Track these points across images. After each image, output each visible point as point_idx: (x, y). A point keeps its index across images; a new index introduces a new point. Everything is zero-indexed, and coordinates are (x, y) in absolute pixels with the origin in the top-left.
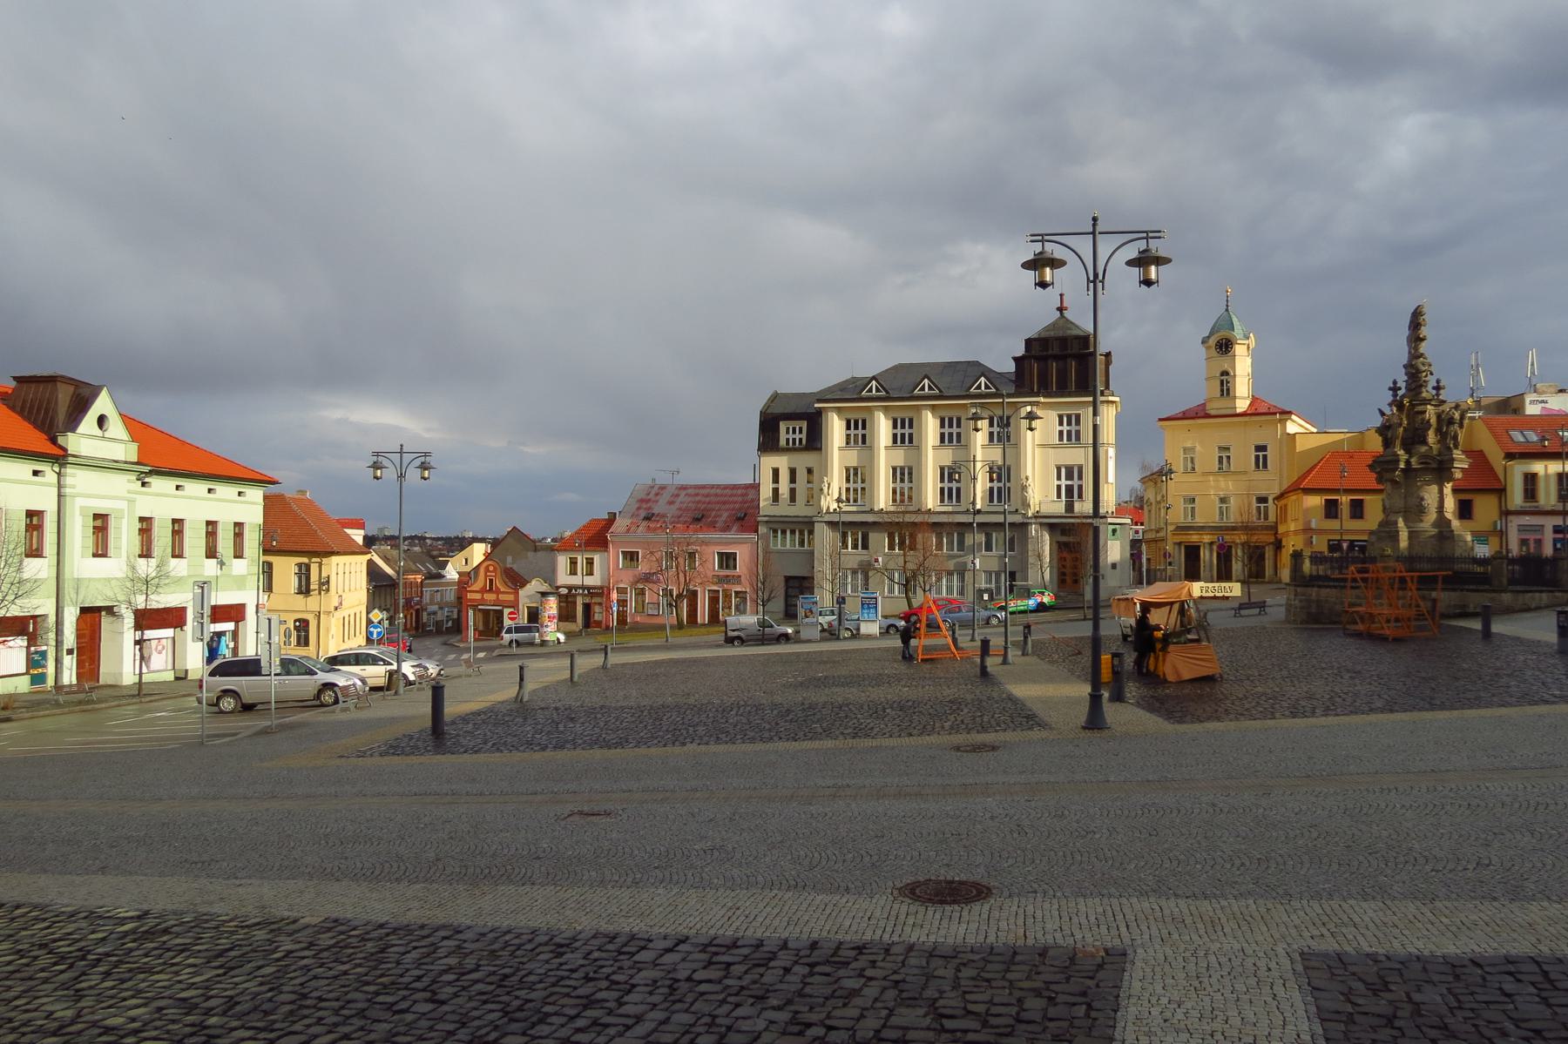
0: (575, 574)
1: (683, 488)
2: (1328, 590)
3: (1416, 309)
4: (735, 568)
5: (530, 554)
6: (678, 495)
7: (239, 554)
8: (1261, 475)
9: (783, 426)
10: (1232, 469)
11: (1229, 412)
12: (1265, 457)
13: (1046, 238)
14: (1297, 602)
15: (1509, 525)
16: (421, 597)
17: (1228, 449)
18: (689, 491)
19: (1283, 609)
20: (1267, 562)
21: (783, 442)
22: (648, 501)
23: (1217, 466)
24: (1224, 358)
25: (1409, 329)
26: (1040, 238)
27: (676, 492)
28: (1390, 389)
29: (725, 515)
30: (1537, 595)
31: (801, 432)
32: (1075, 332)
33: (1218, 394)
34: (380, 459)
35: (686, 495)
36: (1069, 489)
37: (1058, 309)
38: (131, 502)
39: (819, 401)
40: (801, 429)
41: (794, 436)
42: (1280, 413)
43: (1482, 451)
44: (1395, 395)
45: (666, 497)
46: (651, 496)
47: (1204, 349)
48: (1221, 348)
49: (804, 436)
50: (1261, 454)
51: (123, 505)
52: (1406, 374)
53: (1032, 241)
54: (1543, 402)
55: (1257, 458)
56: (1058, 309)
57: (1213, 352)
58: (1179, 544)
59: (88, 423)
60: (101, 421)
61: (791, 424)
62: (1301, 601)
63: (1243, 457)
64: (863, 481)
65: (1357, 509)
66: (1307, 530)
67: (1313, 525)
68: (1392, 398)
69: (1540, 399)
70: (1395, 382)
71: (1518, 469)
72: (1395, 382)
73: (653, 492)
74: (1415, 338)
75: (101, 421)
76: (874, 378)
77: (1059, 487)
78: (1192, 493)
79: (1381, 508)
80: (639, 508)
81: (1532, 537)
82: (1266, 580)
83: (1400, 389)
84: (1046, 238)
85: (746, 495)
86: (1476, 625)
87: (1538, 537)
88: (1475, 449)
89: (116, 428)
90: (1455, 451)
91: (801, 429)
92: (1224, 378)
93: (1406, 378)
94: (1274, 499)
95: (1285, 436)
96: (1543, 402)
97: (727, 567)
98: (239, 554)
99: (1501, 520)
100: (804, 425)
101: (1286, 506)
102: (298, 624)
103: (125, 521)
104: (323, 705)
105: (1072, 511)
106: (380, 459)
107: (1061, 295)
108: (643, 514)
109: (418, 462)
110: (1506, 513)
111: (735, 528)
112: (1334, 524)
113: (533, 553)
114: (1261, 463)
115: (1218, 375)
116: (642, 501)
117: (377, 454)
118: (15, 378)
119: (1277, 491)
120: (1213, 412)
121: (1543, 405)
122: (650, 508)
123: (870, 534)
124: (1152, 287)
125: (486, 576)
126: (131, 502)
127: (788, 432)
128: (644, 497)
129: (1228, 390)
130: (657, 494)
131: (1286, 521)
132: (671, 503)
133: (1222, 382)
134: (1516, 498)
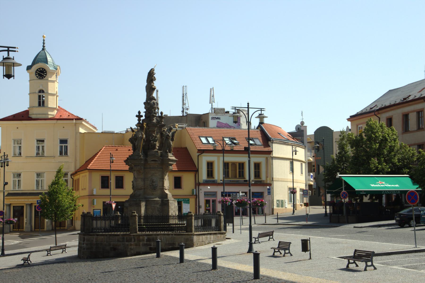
2: (103, 237)
3: (152, 69)
8: (63, 159)
10: (45, 154)
12: (66, 147)
13: (10, 49)
14: (85, 245)
15: (200, 191)
17: (43, 141)
19: (77, 248)
23: (35, 152)
25: (147, 82)
26: (260, 109)
28: (137, 116)
30: (209, 236)
33: (37, 104)
42: (76, 119)
43: (186, 148)
44: (139, 120)
47: (28, 74)
48: (40, 71)
50: (63, 145)
52: (145, 108)
53: (264, 109)
54: (218, 118)
55: (61, 147)
58: (10, 205)
62: (87, 245)
65: (120, 183)
66: (91, 196)
67: (95, 193)
68: (137, 122)
69: (217, 117)
70: (139, 112)
71: (205, 159)
72: (139, 112)
74: (150, 89)
78: (19, 171)
79: (132, 186)
81: (211, 199)
83: (142, 116)
84: (10, 49)
86: (176, 254)
87: (214, 199)
88: (183, 146)
90: (169, 154)
92: (41, 94)
93: (154, 76)
94: (71, 175)
95: (78, 134)
96: (218, 118)
99: (196, 188)
101: (78, 179)
109: (257, 114)
110: (198, 184)
112: (106, 192)
114: (64, 152)
115: (37, 91)
119: (72, 170)
120: (33, 117)
121: (218, 120)
124: (11, 79)
129: (43, 102)
131: (78, 190)
133: (40, 96)
134: (203, 175)
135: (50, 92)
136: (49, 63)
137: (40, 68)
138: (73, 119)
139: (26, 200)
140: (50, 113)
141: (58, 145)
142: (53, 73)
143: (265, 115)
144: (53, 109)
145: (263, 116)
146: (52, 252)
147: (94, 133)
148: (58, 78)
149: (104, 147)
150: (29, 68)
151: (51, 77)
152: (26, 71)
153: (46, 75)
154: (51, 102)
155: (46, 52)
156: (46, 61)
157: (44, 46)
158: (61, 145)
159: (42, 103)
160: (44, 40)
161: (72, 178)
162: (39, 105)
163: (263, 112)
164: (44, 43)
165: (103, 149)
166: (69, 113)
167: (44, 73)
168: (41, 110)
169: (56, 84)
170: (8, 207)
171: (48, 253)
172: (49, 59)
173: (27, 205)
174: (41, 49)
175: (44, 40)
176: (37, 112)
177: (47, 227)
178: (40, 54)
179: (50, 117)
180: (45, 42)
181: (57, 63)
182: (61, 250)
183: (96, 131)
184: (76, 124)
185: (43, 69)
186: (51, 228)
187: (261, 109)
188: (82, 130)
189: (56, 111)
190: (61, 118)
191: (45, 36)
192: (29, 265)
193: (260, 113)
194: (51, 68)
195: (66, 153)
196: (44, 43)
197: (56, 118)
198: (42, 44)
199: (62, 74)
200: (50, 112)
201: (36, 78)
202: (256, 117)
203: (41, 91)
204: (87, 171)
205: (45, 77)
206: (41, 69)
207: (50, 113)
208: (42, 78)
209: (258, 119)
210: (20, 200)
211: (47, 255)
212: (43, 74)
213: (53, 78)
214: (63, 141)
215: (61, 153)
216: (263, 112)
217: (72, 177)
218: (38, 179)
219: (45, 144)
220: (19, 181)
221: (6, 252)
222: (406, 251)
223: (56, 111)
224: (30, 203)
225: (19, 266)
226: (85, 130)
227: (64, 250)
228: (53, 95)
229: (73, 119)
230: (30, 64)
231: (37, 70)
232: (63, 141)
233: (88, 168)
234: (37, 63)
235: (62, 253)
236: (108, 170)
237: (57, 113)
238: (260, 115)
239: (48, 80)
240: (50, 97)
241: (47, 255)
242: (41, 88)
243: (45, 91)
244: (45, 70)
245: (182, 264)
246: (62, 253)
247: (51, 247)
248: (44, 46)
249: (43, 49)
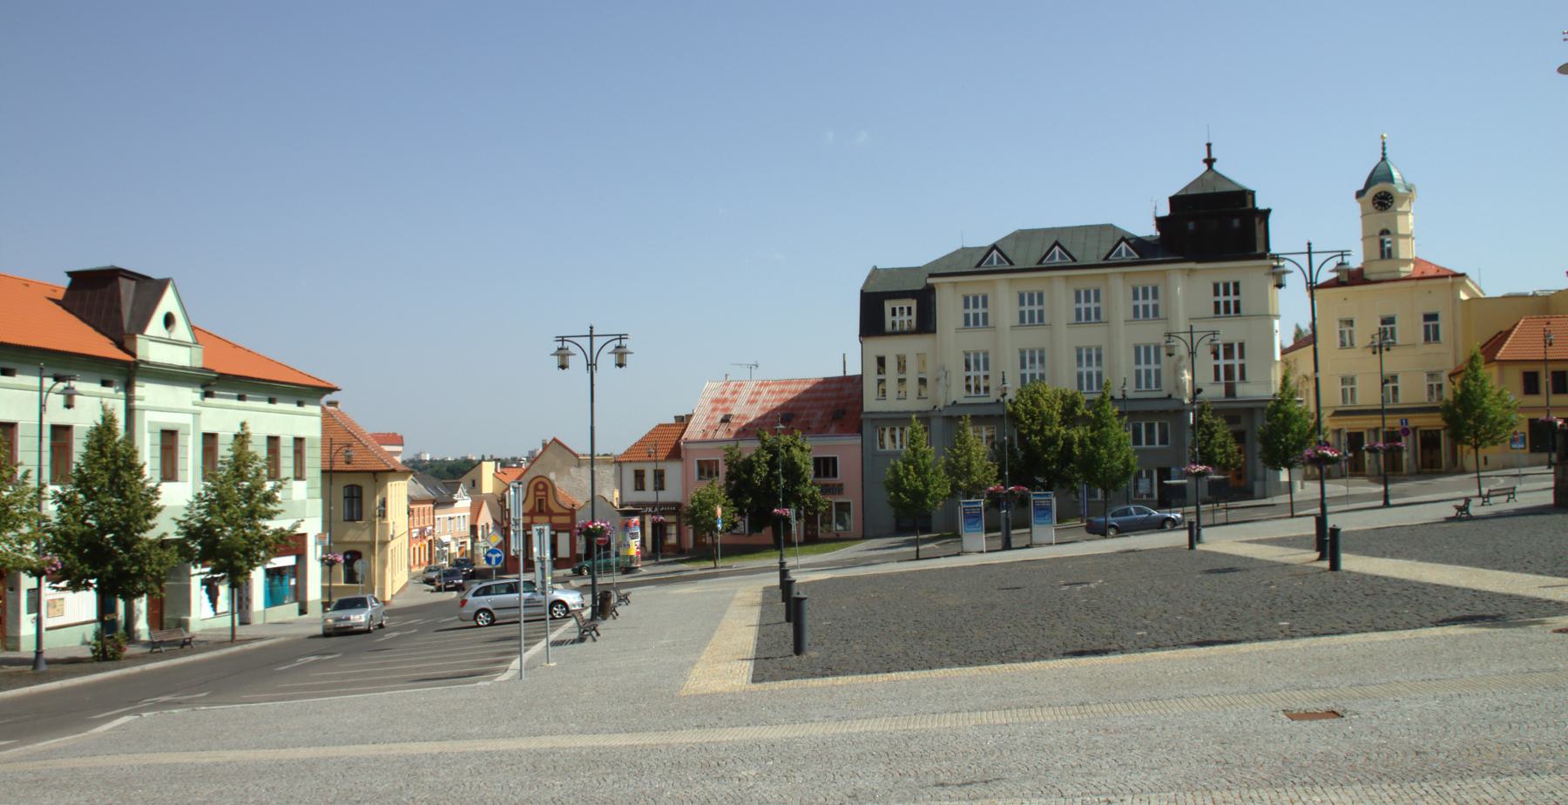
0: (642, 489)
1: (764, 384)
4: (835, 475)
5: (573, 470)
6: (759, 393)
7: (299, 476)
8: (1432, 348)
9: (888, 306)
11: (1391, 276)
12: (1436, 328)
16: (434, 526)
18: (773, 387)
19: (1551, 493)
20: (22, 748)
21: (888, 326)
22: (725, 401)
24: (1385, 215)
27: (736, 396)
29: (820, 413)
31: (909, 313)
32: (1228, 188)
33: (1378, 255)
34: (566, 344)
35: (769, 392)
36: (1229, 370)
37: (1205, 161)
38: (196, 414)
39: (932, 276)
40: (909, 309)
41: (976, 311)
45: (745, 394)
46: (727, 395)
48: (1382, 198)
49: (914, 317)
50: (1431, 323)
51: (186, 419)
55: (1427, 327)
56: (1205, 161)
57: (1370, 207)
59: (155, 326)
60: (169, 320)
61: (897, 304)
63: (1409, 328)
64: (986, 368)
73: (729, 391)
75: (169, 320)
76: (994, 247)
77: (1217, 368)
80: (714, 410)
82: (1443, 469)
85: (841, 389)
89: (181, 331)
91: (909, 309)
97: (826, 475)
98: (299, 476)
100: (913, 304)
102: (348, 557)
103: (190, 438)
104: (479, 626)
105: (1234, 395)
106: (566, 344)
107: (1209, 145)
108: (720, 416)
109: (611, 347)
111: (833, 429)
112: (1532, 400)
113: (576, 469)
114: (1432, 335)
115: (1377, 234)
116: (717, 401)
117: (563, 339)
118: (70, 274)
120: (1373, 277)
122: (727, 409)
123: (1223, 395)
125: (535, 496)
126: (196, 414)
127: (894, 314)
128: (718, 396)
129: (1389, 250)
130: (734, 393)
132: (753, 402)
133: (1382, 243)
135: (1400, 231)
136: (1396, 181)
137: (1380, 193)
138: (1446, 277)
139: (1368, 422)
140: (1402, 269)
141: (1420, 325)
142: (1404, 198)
143: (629, 348)
144: (1407, 262)
145: (566, 352)
146: (1492, 500)
147: (1480, 298)
148: (1412, 207)
149: (1523, 320)
150: (1360, 194)
151: (1401, 206)
152: (1355, 200)
153: (1392, 202)
154: (1406, 250)
155: (1389, 163)
156: (1390, 179)
157: (1384, 154)
158: (1426, 323)
159: (1386, 253)
160: (1384, 143)
161: (1451, 381)
162: (1382, 256)
163: (624, 342)
164: (1384, 149)
165: (1521, 323)
166: (1437, 266)
167: (1387, 199)
168: (1385, 265)
169: (1411, 218)
170: (1335, 436)
171: (1484, 502)
172: (1395, 174)
173: (1369, 430)
174: (1379, 159)
175: (1384, 143)
176: (1379, 268)
177: (1408, 466)
178: (1378, 168)
179: (1403, 275)
180: (1386, 145)
181: (1408, 181)
182: (1506, 497)
183: (1482, 296)
184: (1452, 284)
185: (1385, 192)
186: (1415, 470)
187: (621, 335)
188: (1463, 296)
189: (1412, 265)
190: (1425, 275)
191: (1385, 135)
192: (1471, 518)
193: (560, 346)
194: (1401, 190)
195: (1436, 338)
196: (1384, 149)
197: (1414, 276)
198: (1381, 151)
199: (1420, 195)
200: (139, 380)
201: (1374, 210)
202: (610, 353)
203: (1385, 232)
204: (1495, 363)
205: (1389, 207)
206: (1383, 194)
207: (1402, 269)
208: (1386, 209)
209: (556, 357)
210: (1356, 422)
211: (1483, 505)
212: (1386, 202)
213: (1405, 207)
214: (1431, 317)
215: (1427, 338)
216: (624, 342)
217: (1453, 379)
218: (1344, 387)
219: (1398, 326)
220: (1352, 390)
221: (1392, 502)
222: (10, 749)
223: (1412, 265)
224: (1373, 426)
225: (1449, 520)
226: (1467, 294)
227: (1512, 496)
228: (1406, 236)
229: (1446, 277)
230: (1361, 187)
231: (1376, 196)
232: (1431, 317)
233: (1497, 358)
234: (1375, 183)
235: (1508, 501)
236: (1542, 360)
237: (1414, 268)
238: (560, 349)
239: (1395, 211)
240: (1401, 242)
241: (1483, 505)
242: (1384, 226)
243: (1392, 232)
244: (1389, 194)
245: (1335, 573)
246: (1508, 501)
247: (1490, 491)
248: (1384, 154)
249: (1383, 159)
